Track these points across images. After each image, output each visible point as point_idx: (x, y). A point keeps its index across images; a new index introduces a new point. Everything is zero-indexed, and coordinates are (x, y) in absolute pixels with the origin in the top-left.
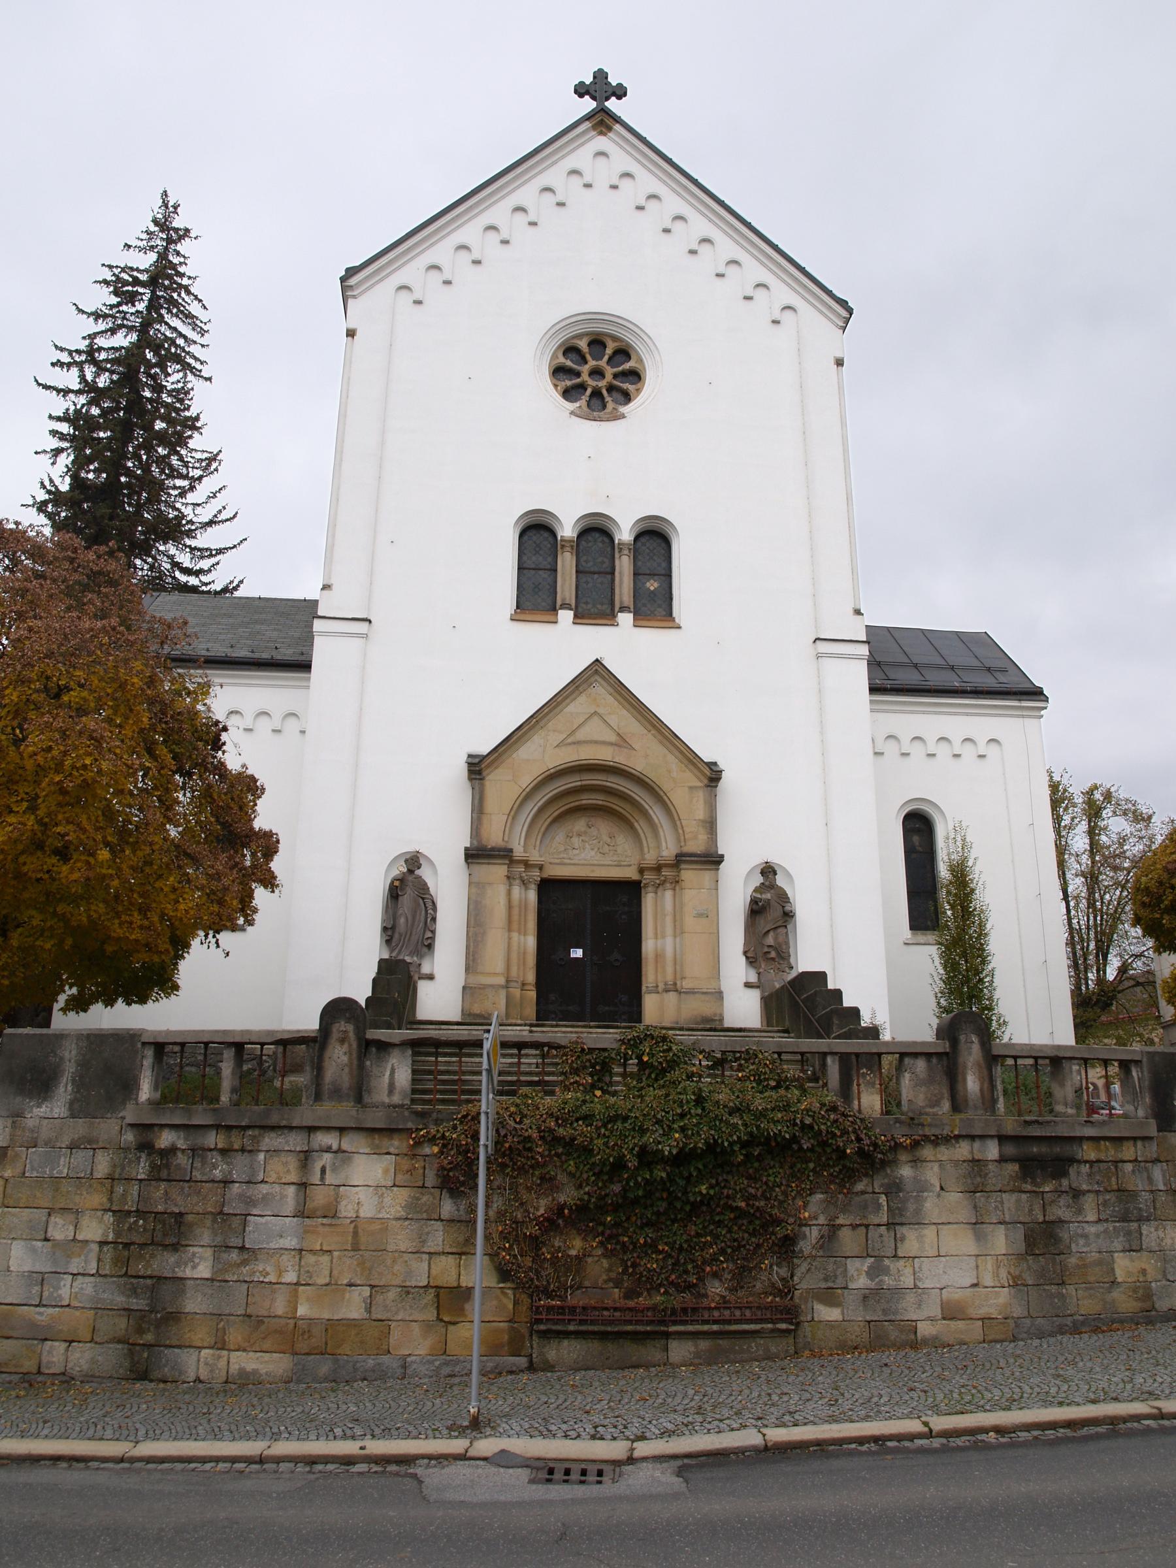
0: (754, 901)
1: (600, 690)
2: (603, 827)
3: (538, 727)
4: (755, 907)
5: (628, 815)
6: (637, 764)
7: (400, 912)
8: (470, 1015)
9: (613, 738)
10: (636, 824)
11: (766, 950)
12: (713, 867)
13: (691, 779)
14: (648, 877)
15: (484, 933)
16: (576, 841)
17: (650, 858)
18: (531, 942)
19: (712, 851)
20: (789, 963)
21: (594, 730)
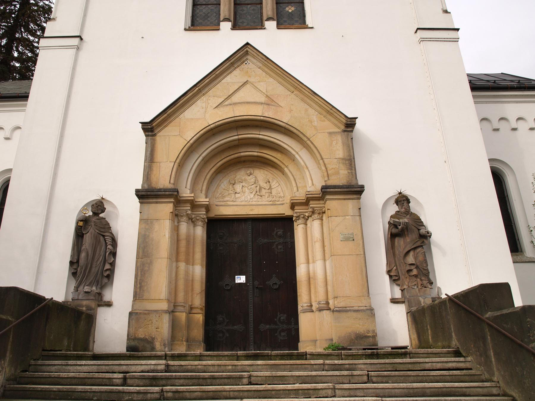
0: (393, 225)
2: (261, 175)
4: (394, 231)
5: (278, 162)
6: (283, 117)
7: (83, 248)
8: (135, 339)
9: (263, 99)
10: (286, 169)
11: (408, 268)
12: (355, 196)
15: (151, 263)
18: (198, 271)
19: (354, 183)
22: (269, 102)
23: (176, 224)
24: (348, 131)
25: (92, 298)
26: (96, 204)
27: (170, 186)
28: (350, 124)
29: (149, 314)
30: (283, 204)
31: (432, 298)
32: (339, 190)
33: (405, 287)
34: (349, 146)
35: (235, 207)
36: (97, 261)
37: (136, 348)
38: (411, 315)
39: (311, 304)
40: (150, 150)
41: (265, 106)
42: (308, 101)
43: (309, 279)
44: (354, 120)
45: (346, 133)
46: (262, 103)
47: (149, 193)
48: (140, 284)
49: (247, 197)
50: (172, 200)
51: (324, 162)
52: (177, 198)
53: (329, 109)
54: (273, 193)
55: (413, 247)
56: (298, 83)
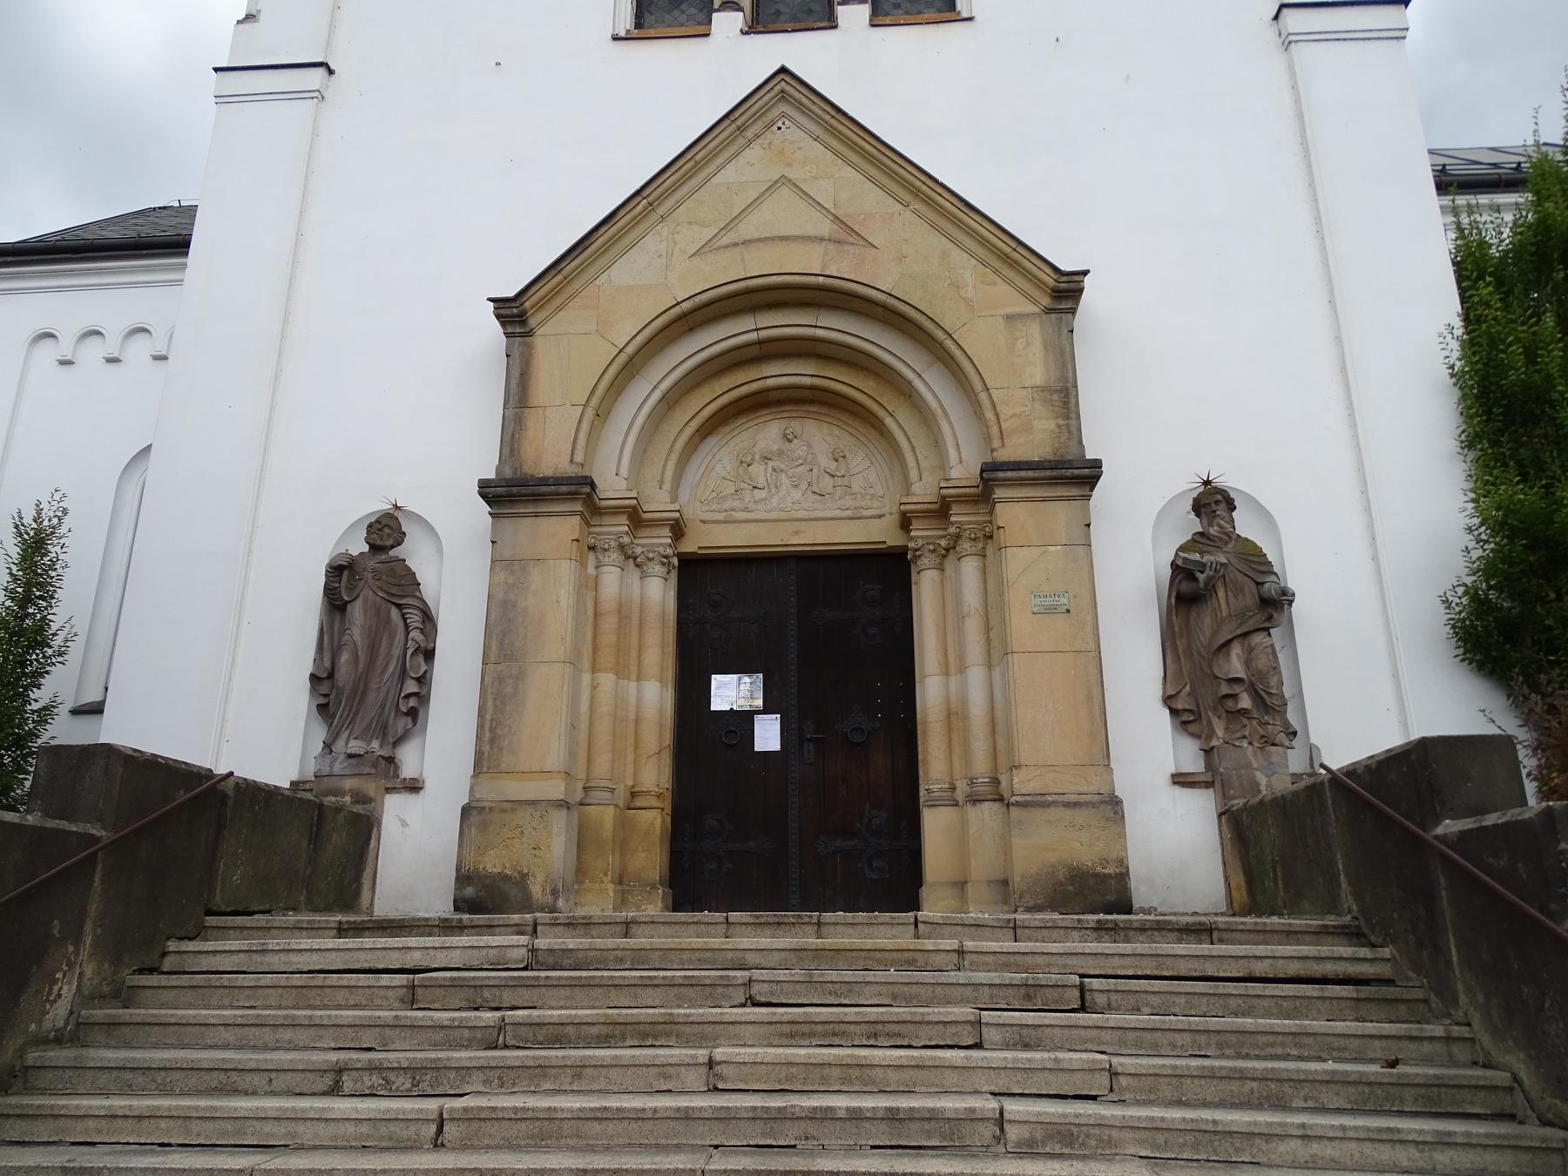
0: (1182, 571)
1: (795, 141)
2: (819, 437)
3: (654, 217)
4: (1186, 587)
6: (882, 275)
9: (825, 227)
10: (888, 421)
11: (1225, 689)
12: (1075, 491)
13: (1008, 297)
14: (921, 532)
15: (521, 676)
16: (759, 472)
17: (924, 491)
20: (1287, 724)
21: (783, 214)
22: (843, 236)
23: (591, 571)
24: (1060, 311)
25: (367, 770)
26: (378, 521)
27: (571, 471)
28: (1066, 291)
29: (513, 810)
30: (880, 516)
31: (1293, 775)
32: (1030, 474)
33: (1214, 743)
34: (1062, 353)
35: (750, 526)
36: (383, 672)
37: (482, 896)
38: (1229, 820)
39: (952, 784)
40: (517, 374)
41: (831, 247)
42: (950, 229)
43: (949, 716)
44: (1077, 278)
45: (1054, 316)
46: (822, 240)
47: (514, 490)
48: (492, 730)
49: (789, 493)
50: (578, 507)
51: (990, 397)
52: (593, 502)
53: (1008, 250)
54: (856, 488)
55: (1239, 632)
56: (923, 178)
